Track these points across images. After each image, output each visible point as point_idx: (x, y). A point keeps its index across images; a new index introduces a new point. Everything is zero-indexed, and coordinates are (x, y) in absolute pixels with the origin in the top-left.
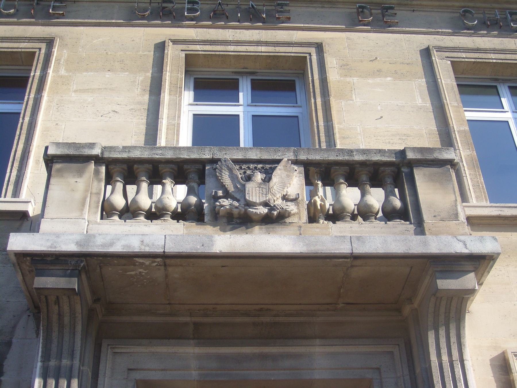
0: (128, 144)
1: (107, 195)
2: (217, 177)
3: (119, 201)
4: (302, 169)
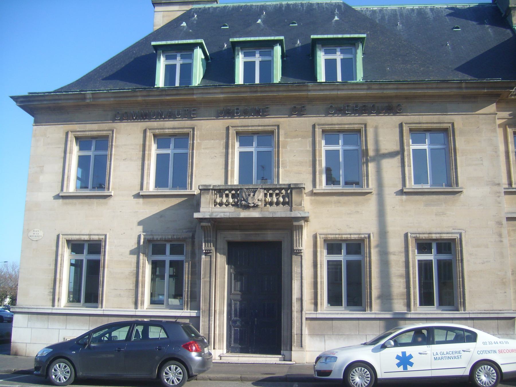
0: (220, 184)
1: (215, 199)
2: (242, 194)
3: (218, 200)
4: (190, 375)
